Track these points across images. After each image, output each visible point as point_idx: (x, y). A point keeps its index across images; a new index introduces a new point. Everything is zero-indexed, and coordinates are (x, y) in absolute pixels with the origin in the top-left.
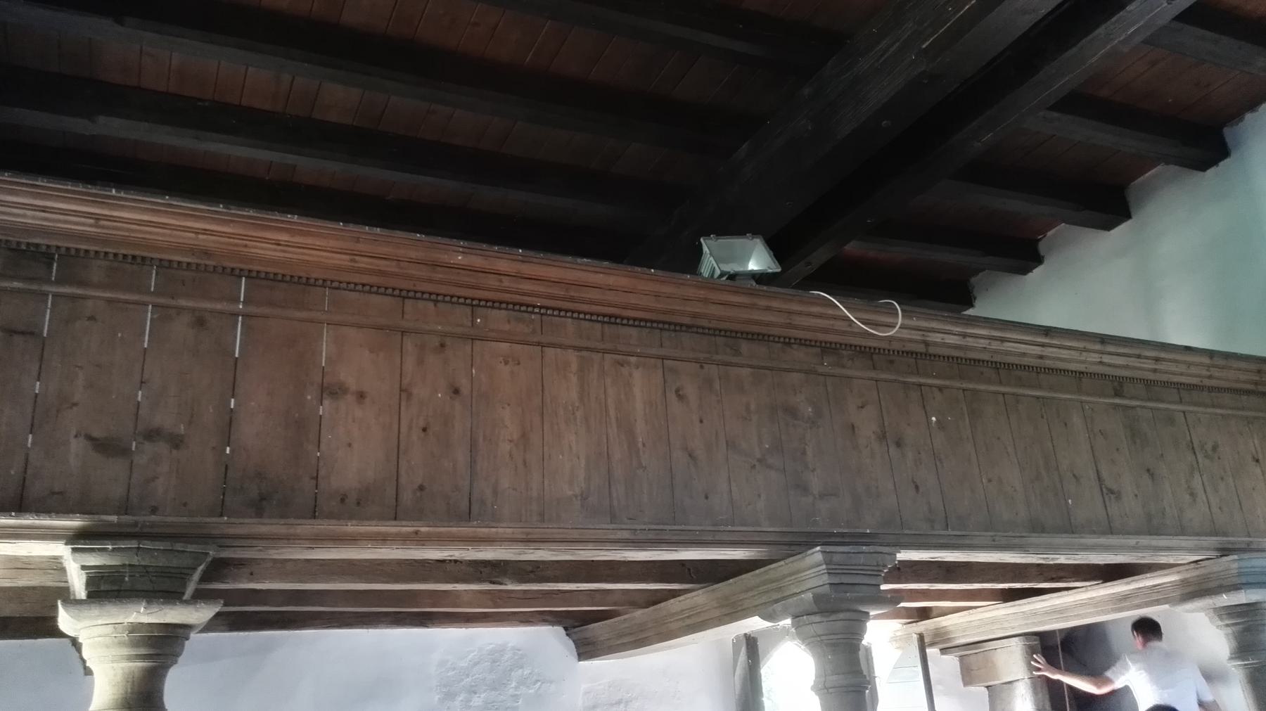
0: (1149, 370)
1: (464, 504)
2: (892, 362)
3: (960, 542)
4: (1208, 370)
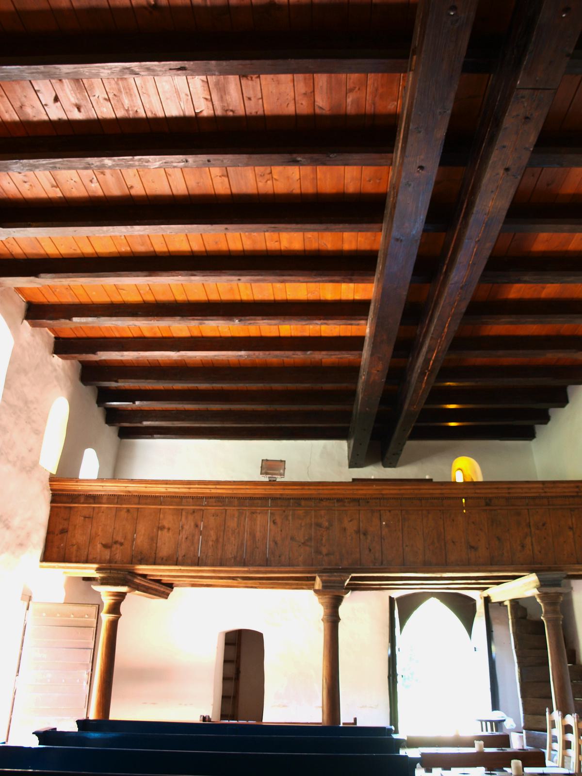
0: (506, 493)
1: (197, 561)
2: (368, 502)
3: (384, 570)
4: (543, 489)
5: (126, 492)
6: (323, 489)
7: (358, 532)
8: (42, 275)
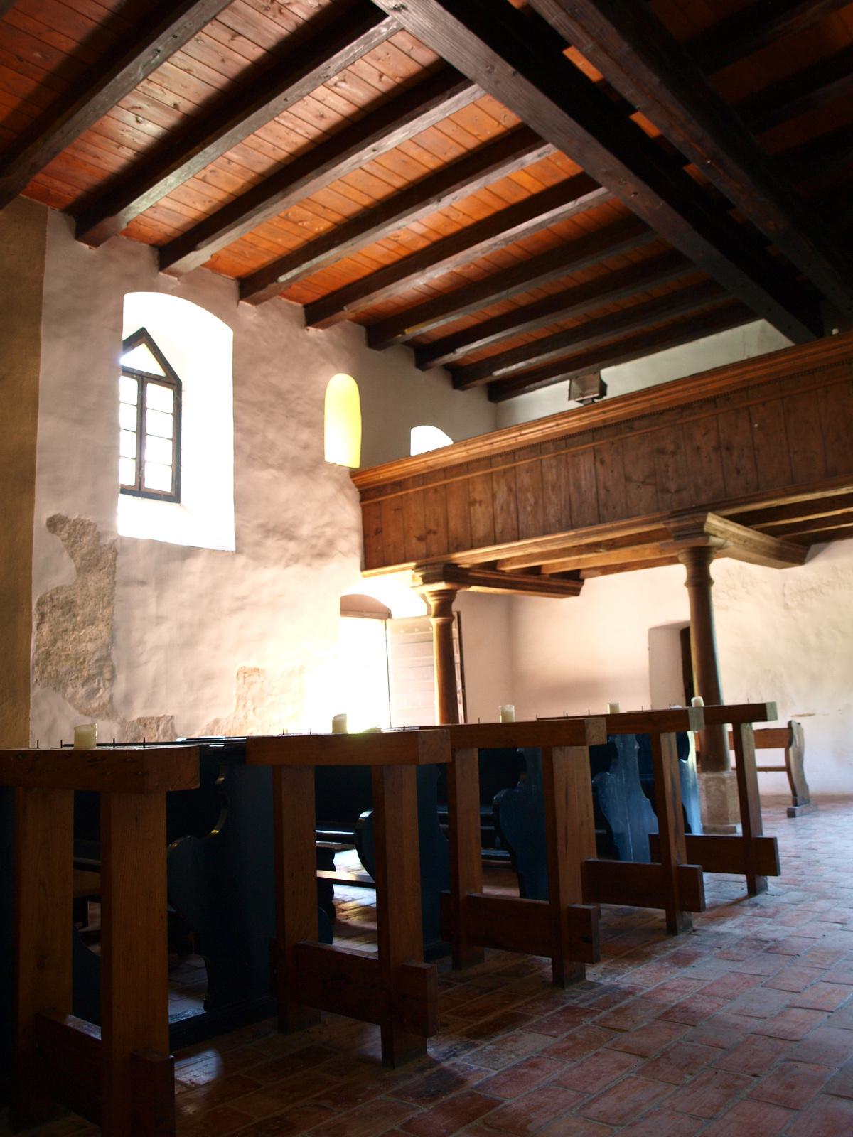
5: (428, 467)
6: (656, 398)
7: (717, 448)
8: (199, 245)
